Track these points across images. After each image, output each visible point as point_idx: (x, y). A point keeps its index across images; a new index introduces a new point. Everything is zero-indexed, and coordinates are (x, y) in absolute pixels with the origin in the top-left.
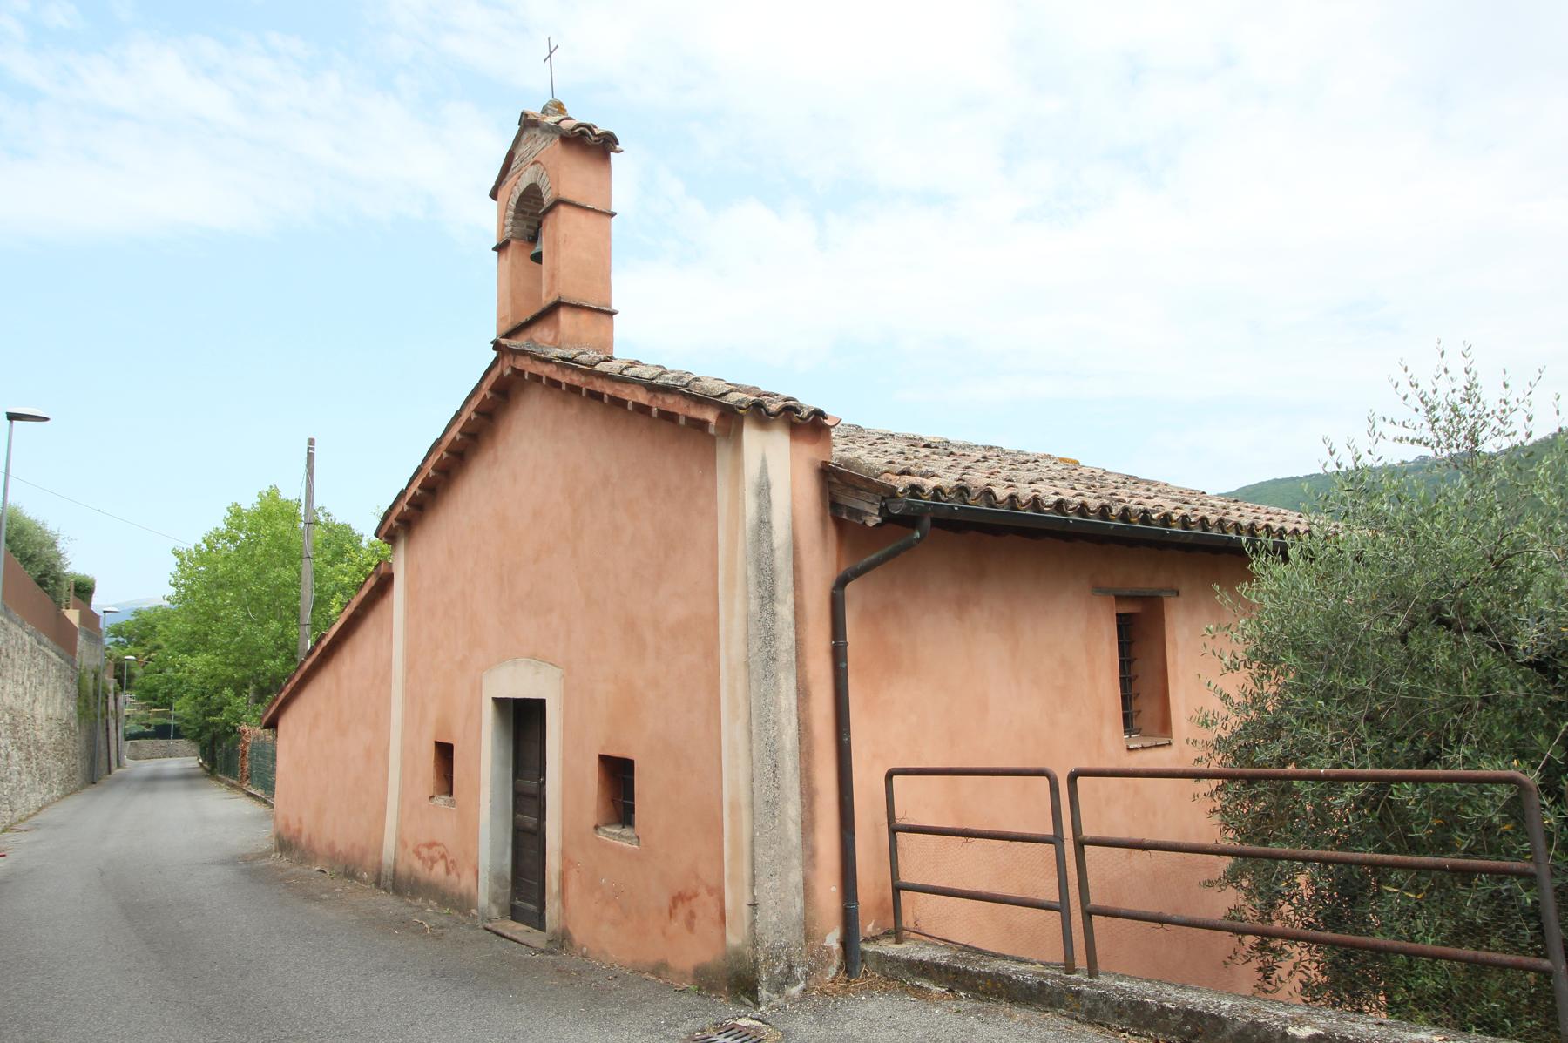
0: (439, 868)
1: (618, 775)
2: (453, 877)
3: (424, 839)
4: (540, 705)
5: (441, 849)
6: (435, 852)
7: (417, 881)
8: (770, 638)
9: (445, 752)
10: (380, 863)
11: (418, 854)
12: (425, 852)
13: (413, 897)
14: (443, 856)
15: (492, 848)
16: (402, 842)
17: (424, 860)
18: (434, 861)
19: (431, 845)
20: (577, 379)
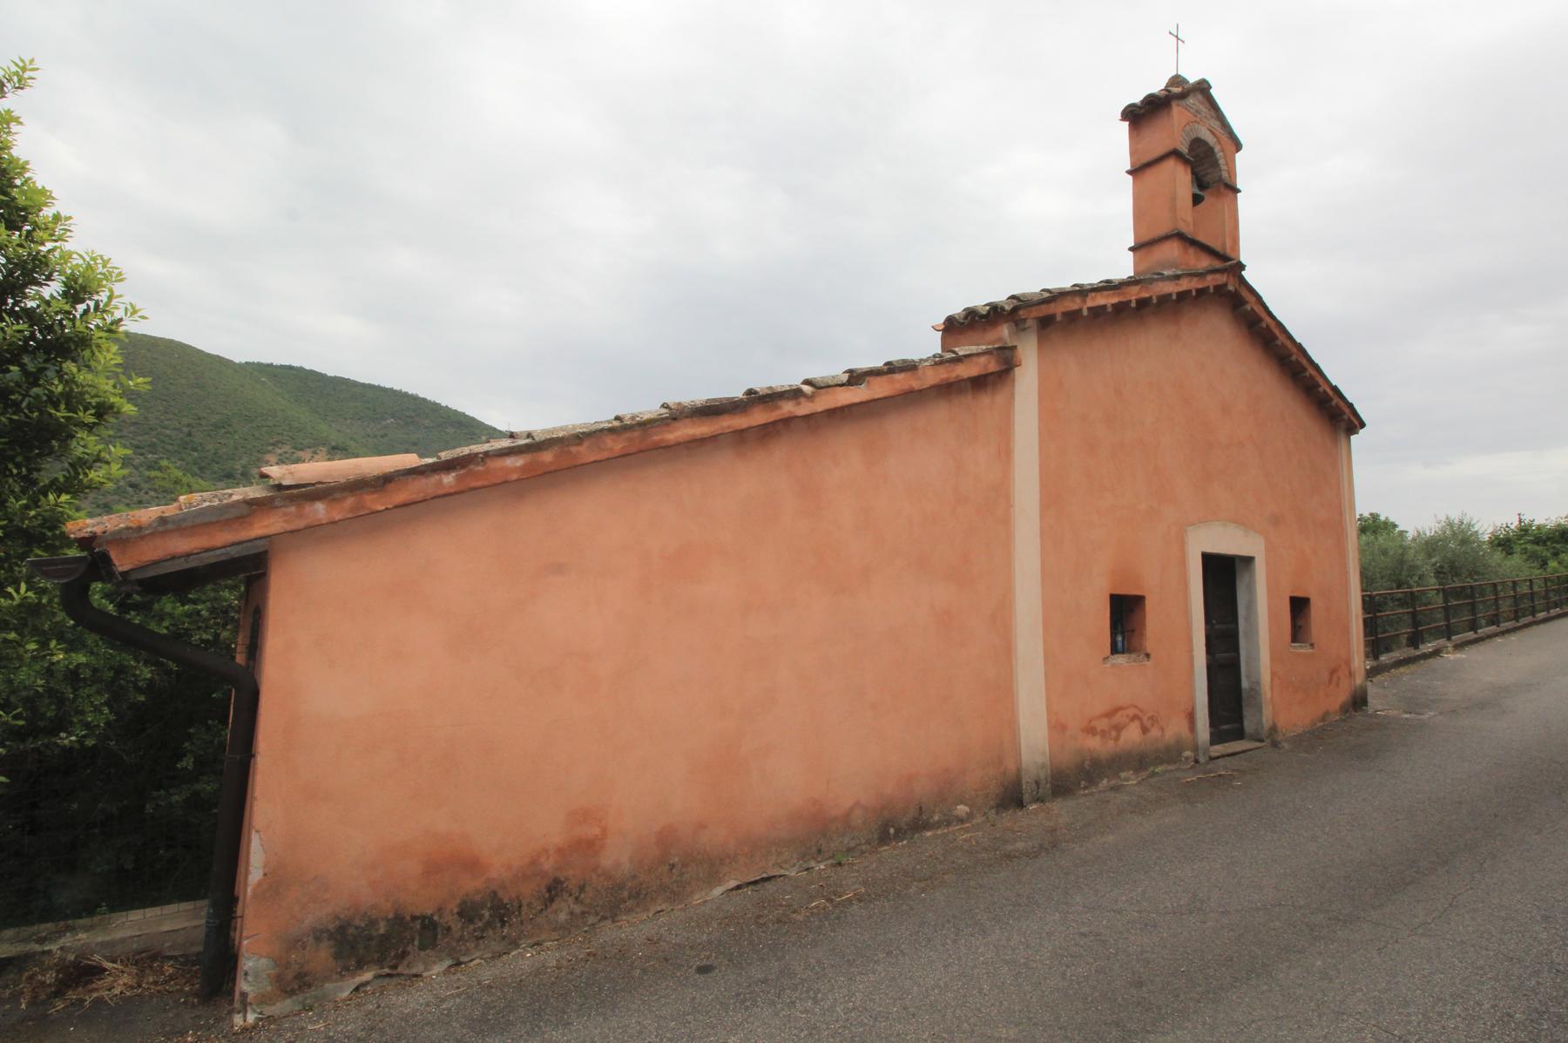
1: (1299, 606)
2: (1155, 732)
5: (1131, 712)
6: (1119, 718)
8: (740, 435)
10: (1019, 770)
14: (1135, 718)
17: (1103, 734)
18: (1119, 728)
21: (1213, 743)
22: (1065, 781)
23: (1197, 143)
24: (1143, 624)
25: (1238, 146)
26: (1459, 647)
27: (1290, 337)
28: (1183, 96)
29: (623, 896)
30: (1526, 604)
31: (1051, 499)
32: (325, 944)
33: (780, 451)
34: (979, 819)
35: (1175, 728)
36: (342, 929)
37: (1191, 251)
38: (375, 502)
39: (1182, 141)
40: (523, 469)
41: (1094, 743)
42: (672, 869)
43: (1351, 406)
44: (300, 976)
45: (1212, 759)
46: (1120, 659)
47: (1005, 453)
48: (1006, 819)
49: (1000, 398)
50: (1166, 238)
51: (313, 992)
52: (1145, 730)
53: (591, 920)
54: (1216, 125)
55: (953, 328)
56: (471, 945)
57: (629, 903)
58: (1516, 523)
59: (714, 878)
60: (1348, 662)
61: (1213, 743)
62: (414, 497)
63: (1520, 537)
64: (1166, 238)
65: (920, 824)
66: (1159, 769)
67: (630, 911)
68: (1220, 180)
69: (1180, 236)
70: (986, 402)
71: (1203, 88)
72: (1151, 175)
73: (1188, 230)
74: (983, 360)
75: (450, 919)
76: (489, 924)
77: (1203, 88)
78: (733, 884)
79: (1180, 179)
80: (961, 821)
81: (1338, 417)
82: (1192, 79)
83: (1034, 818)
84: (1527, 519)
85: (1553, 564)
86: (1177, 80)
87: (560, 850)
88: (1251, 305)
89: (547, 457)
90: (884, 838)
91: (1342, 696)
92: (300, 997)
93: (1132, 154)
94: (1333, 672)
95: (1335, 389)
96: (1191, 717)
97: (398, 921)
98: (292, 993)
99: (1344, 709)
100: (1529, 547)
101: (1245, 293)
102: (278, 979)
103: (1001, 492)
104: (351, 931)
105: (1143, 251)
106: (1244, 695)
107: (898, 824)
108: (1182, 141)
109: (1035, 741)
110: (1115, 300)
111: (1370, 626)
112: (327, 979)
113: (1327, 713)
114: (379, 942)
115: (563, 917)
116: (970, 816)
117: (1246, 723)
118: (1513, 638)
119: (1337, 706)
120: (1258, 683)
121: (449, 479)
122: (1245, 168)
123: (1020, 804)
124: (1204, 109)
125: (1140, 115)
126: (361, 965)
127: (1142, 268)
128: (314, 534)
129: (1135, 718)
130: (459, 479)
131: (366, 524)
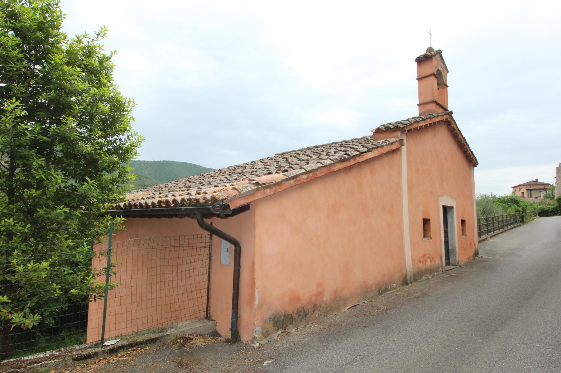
0: (428, 263)
1: (463, 222)
2: (433, 262)
3: (422, 254)
4: (452, 208)
5: (428, 256)
6: (426, 258)
7: (421, 271)
8: (351, 167)
9: (426, 222)
10: (406, 273)
11: (420, 261)
12: (422, 260)
13: (421, 278)
14: (429, 258)
15: (458, 234)
16: (413, 260)
17: (423, 263)
18: (426, 261)
19: (424, 256)
20: (429, 122)
21: (446, 266)
22: (418, 276)
23: (438, 71)
24: (430, 228)
25: (448, 72)
26: (491, 237)
27: (462, 135)
28: (435, 55)
29: (329, 309)
30: (505, 224)
31: (410, 189)
32: (272, 322)
33: (354, 173)
34: (398, 289)
35: (438, 261)
36: (274, 318)
37: (438, 107)
38: (279, 189)
39: (432, 67)
40: (307, 178)
41: (421, 265)
42: (339, 300)
43: (475, 158)
44: (267, 332)
45: (446, 271)
46: (425, 239)
47: (400, 173)
48: (405, 288)
49: (398, 155)
50: (431, 102)
51: (270, 337)
52: (431, 262)
53: (323, 316)
54: (442, 64)
55: (378, 131)
56: (299, 323)
57: (330, 312)
58: (490, 195)
59: (345, 305)
60: (474, 241)
61: (446, 266)
62: (287, 187)
63: (498, 201)
64: (431, 102)
65: (386, 290)
66: (435, 274)
67: (330, 314)
68: (443, 83)
69: (436, 102)
70: (396, 156)
71: (439, 52)
72: (425, 81)
73: (437, 100)
74: (397, 143)
75: (295, 316)
76: (303, 317)
77: (439, 52)
78: (349, 307)
79: (433, 81)
80: (395, 289)
81: (471, 161)
82: (436, 49)
83: (415, 288)
84: (494, 194)
85: (509, 210)
86: (430, 49)
87: (315, 295)
88: (453, 125)
89: (311, 175)
90: (379, 294)
91: (473, 252)
92: (267, 338)
93: (418, 73)
94: (471, 244)
95: (472, 152)
96: (441, 257)
97: (285, 316)
98: (265, 337)
99: (473, 256)
100: (501, 204)
101: (452, 121)
102: (263, 333)
103: (399, 185)
104: (276, 319)
105: (422, 106)
106: (450, 251)
107: (383, 290)
108: (432, 67)
109: (409, 266)
110: (424, 124)
111: (479, 227)
112: (272, 333)
113: (469, 257)
114: (282, 322)
115: (317, 315)
116: (396, 287)
117: (450, 260)
118: (505, 234)
119: (471, 255)
120: (455, 247)
121: (292, 182)
122: (450, 79)
123: (407, 284)
124: (439, 59)
125: (421, 61)
126: (279, 329)
127: (422, 111)
128: (266, 199)
129: (429, 258)
130: (294, 182)
131: (276, 196)
